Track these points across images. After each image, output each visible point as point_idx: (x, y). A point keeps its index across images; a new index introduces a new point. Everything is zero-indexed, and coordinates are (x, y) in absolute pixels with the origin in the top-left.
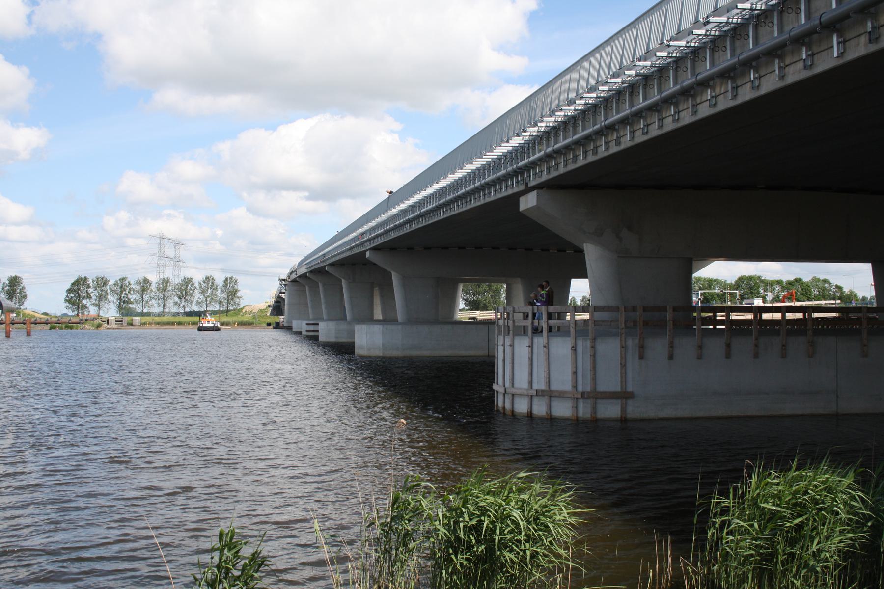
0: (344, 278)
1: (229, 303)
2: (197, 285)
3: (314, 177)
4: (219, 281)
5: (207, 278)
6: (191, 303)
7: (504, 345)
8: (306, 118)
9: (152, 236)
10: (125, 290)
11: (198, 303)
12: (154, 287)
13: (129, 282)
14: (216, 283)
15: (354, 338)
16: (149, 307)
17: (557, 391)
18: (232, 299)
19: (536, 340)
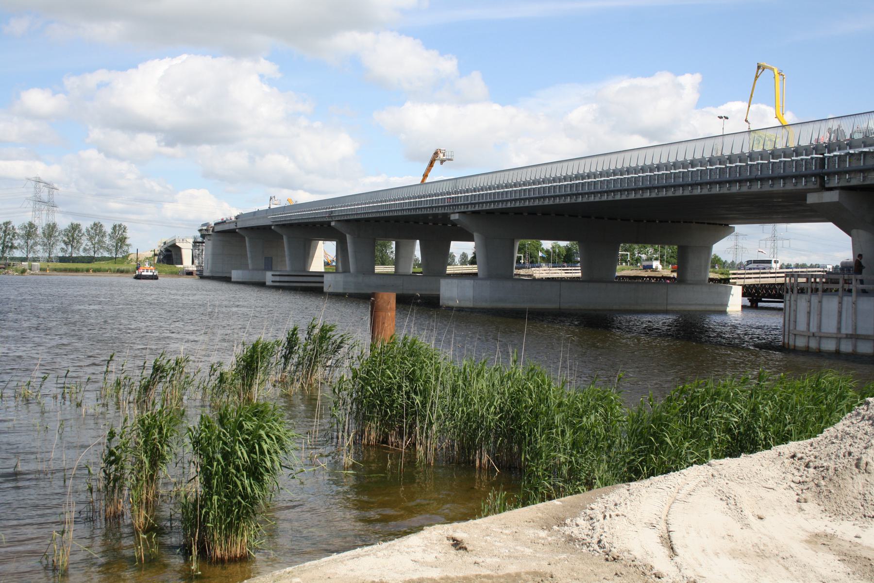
0: (349, 234)
1: (117, 251)
2: (84, 230)
3: (172, 117)
4: (108, 229)
5: (95, 224)
6: (78, 250)
7: (790, 300)
8: (214, 57)
9: (29, 179)
10: (9, 234)
11: (85, 250)
12: (39, 231)
13: (13, 227)
14: (104, 229)
15: (439, 291)
16: (34, 252)
17: (862, 335)
18: (121, 247)
19: (845, 299)
